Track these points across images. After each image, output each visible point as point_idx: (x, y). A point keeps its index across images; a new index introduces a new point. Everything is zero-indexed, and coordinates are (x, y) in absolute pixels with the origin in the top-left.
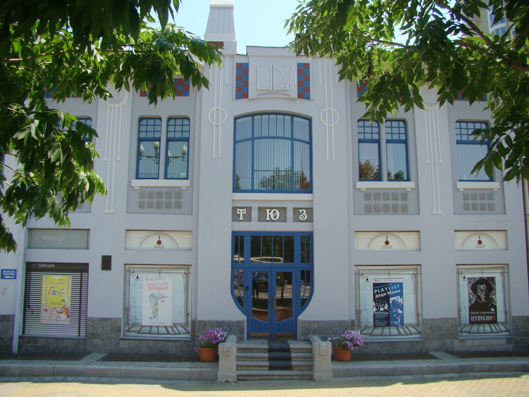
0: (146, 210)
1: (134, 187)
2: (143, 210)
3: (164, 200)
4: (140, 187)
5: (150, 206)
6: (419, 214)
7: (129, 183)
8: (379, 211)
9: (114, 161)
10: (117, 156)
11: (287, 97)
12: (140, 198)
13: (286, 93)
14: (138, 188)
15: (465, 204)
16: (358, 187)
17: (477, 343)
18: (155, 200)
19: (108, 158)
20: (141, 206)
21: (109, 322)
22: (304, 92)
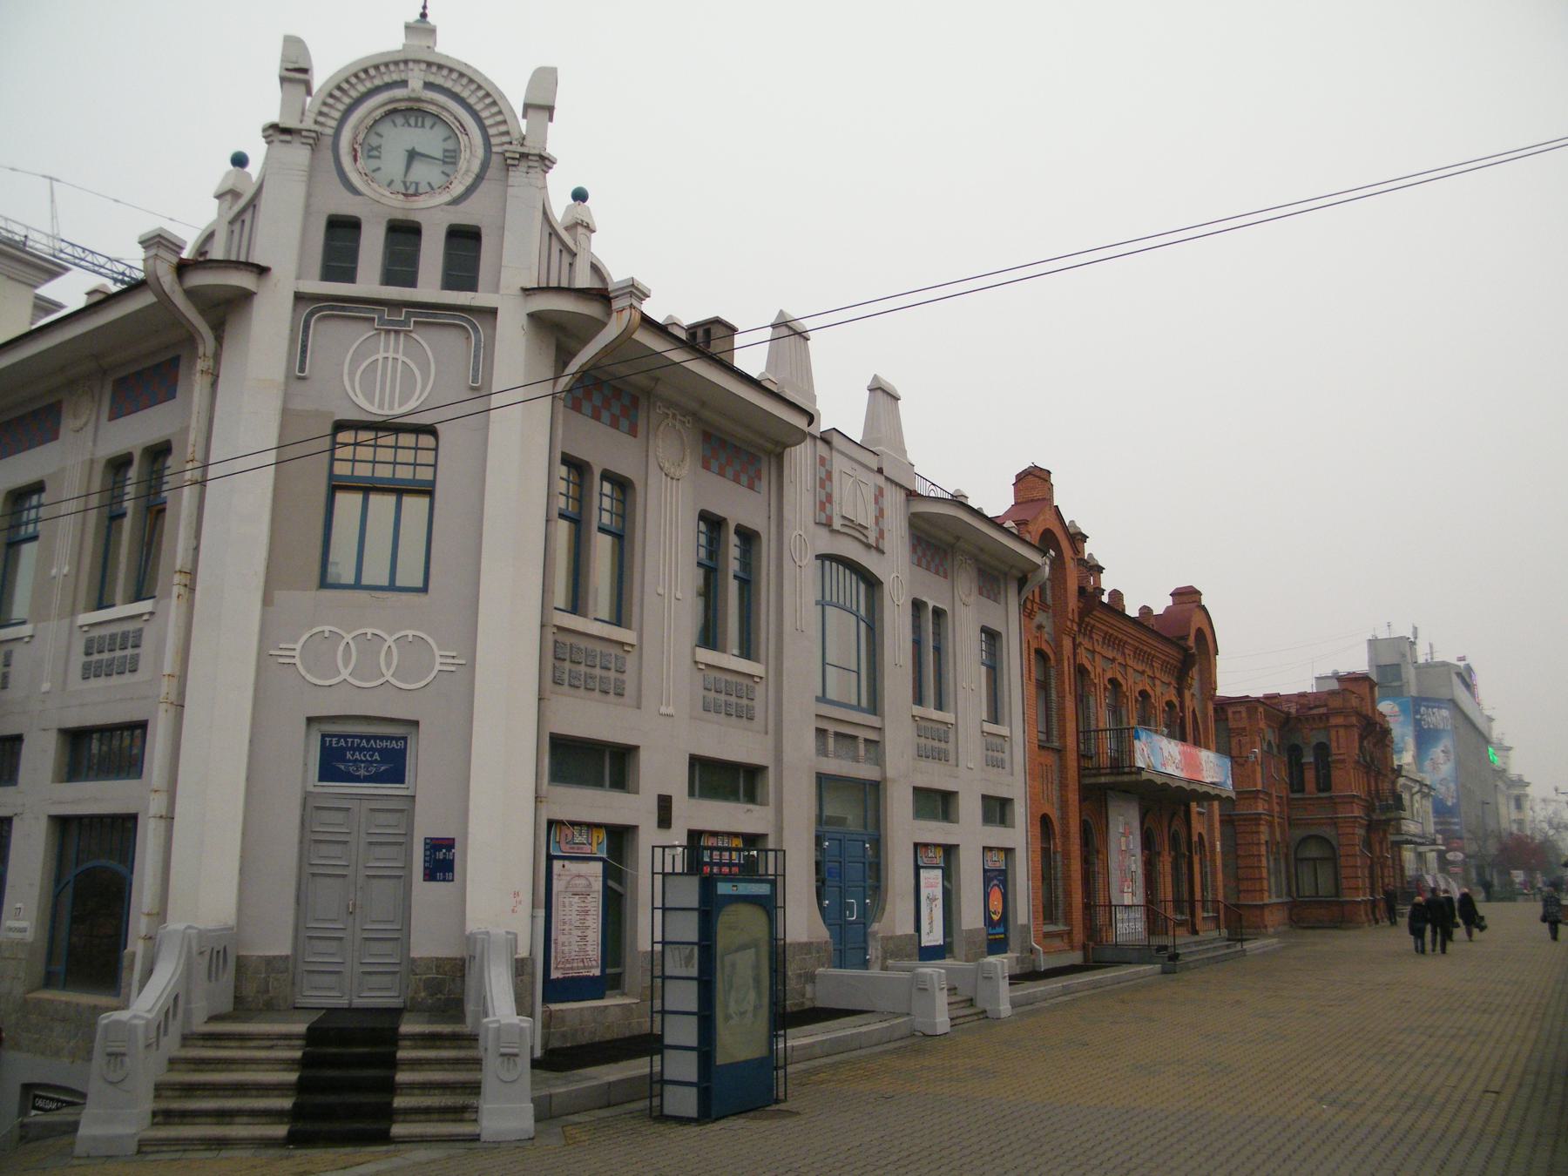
2: (558, 688)
4: (707, 665)
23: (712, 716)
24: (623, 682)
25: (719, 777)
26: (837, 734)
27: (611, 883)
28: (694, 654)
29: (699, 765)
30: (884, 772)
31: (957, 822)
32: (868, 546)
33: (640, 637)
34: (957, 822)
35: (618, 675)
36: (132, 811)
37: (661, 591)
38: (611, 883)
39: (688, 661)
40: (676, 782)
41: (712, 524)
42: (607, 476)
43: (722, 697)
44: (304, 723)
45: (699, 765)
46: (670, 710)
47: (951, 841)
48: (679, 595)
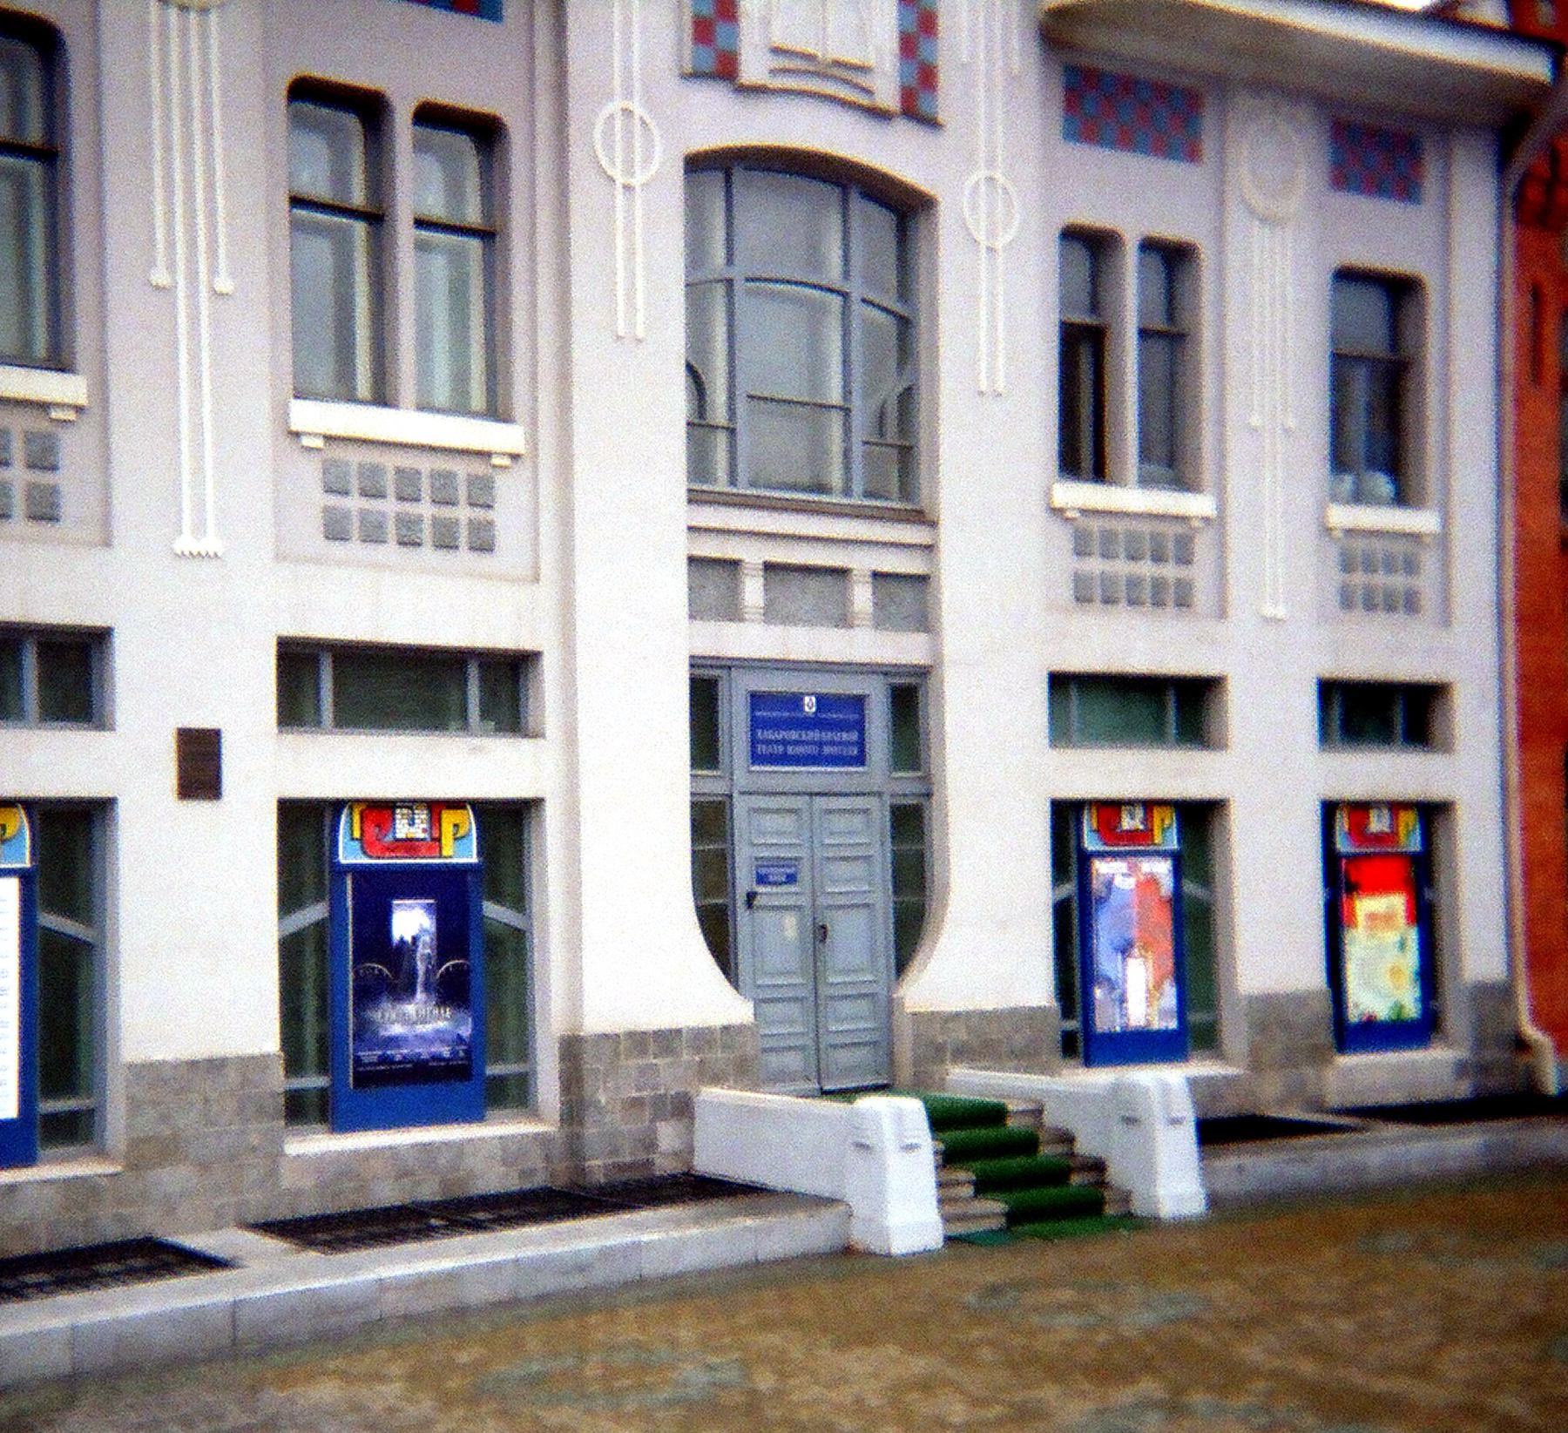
0: (428, 554)
1: (297, 435)
2: (337, 549)
3: (425, 509)
4: (328, 438)
5: (373, 534)
6: (107, 543)
7: (283, 415)
8: (1090, 601)
9: (204, 293)
10: (213, 271)
11: (864, 100)
12: (329, 490)
13: (862, 80)
14: (319, 443)
15: (924, 621)
16: (1058, 502)
17: (923, 300)
18: (390, 506)
19: (171, 267)
20: (335, 530)
21: (233, 1076)
22: (917, 105)
23: (1381, 617)
24: (54, 491)
25: (1369, 711)
26: (769, 567)
27: (49, 920)
28: (1048, 493)
29: (298, 662)
30: (936, 651)
31: (112, 729)
32: (879, 114)
33: (1446, 521)
34: (112, 729)
35: (479, 513)
36: (1047, 808)
37: (160, 277)
38: (49, 920)
39: (1037, 508)
40: (243, 705)
41: (1090, 245)
42: (431, 116)
43: (1146, 569)
44: (1041, 690)
45: (298, 662)
46: (1281, 612)
47: (1436, 791)
48: (224, 284)
